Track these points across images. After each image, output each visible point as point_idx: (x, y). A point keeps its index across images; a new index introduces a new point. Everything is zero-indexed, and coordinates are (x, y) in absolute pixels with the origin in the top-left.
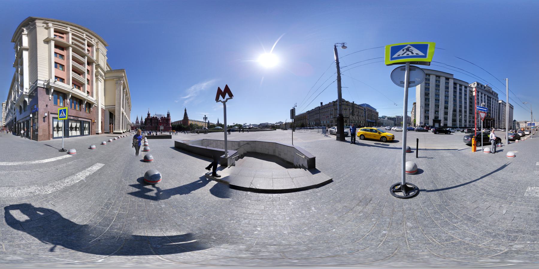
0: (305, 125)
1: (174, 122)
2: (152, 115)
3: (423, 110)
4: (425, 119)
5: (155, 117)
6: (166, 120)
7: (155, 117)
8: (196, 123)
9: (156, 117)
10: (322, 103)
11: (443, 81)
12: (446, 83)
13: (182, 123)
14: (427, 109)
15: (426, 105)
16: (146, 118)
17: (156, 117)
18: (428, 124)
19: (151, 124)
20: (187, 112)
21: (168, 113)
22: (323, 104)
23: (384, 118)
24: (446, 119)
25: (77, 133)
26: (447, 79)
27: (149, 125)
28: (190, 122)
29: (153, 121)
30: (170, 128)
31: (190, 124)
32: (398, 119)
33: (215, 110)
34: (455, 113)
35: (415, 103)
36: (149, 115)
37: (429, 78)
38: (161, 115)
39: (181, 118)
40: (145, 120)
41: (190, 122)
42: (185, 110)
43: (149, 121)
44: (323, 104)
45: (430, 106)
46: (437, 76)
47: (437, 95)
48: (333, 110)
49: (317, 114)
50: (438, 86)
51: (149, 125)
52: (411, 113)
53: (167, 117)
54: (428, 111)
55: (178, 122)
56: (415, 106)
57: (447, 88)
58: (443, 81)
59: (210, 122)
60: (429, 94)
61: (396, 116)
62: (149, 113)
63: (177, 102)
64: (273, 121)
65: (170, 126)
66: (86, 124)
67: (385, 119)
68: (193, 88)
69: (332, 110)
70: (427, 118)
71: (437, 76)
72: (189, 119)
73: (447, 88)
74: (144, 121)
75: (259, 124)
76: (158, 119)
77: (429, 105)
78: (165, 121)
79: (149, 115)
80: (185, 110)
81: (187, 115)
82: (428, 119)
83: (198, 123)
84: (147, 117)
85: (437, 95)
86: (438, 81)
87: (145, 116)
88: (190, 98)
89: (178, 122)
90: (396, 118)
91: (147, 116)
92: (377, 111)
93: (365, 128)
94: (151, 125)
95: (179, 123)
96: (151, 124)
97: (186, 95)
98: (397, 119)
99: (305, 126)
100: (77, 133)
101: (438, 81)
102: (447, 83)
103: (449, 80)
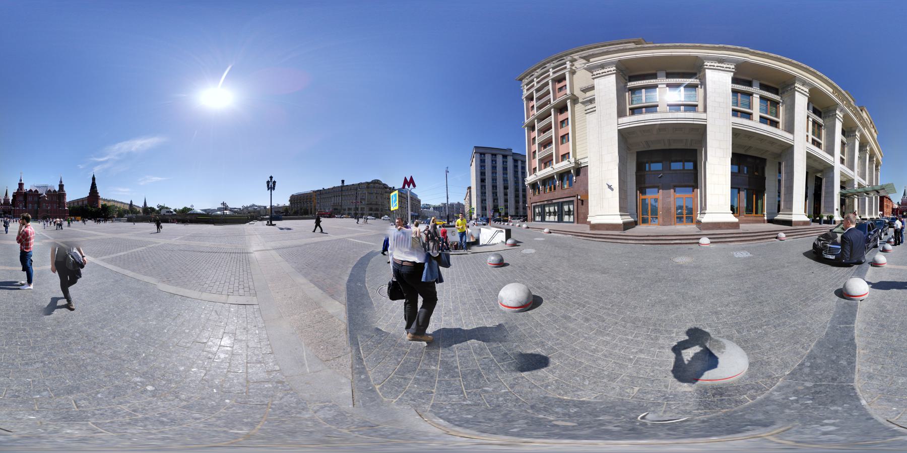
0: (309, 211)
1: (73, 202)
2: (27, 187)
3: (479, 200)
4: (482, 210)
5: (33, 190)
6: (58, 195)
7: (33, 190)
8: (113, 203)
9: (36, 191)
10: (343, 181)
11: (500, 159)
12: (503, 162)
13: (86, 202)
14: (484, 198)
15: (482, 193)
16: (14, 193)
17: (36, 191)
18: (486, 215)
19: (26, 204)
20: (97, 182)
21: (61, 182)
22: (345, 184)
23: (429, 209)
24: (506, 207)
25: (549, 209)
26: (505, 157)
27: (21, 206)
28: (101, 203)
29: (30, 199)
30: (65, 213)
31: (103, 206)
32: (445, 208)
33: (142, 184)
34: (517, 199)
35: (470, 188)
36: (21, 185)
37: (484, 158)
38: (46, 187)
39: (85, 193)
40: (13, 196)
41: (101, 203)
42: (94, 179)
43: (21, 198)
44: (345, 184)
45: (487, 195)
46: (492, 155)
47: (494, 180)
48: (366, 194)
49: (337, 196)
50: (494, 168)
51: (21, 206)
52: (465, 199)
53: (59, 191)
54: (485, 200)
55: (78, 201)
56: (470, 192)
57: (505, 169)
58: (500, 159)
59: (133, 204)
60: (485, 179)
61: (442, 204)
62: (22, 182)
63: (81, 167)
64: (237, 203)
65: (66, 208)
66: (550, 208)
67: (431, 210)
68: (117, 146)
69: (365, 193)
70: (484, 209)
71: (492, 155)
72: (99, 195)
73: (505, 169)
74: (11, 198)
75: (181, 208)
76: (42, 194)
77: (485, 193)
78: (55, 199)
79: (21, 185)
80: (94, 179)
81: (95, 184)
82: (486, 210)
83: (116, 204)
84: (18, 190)
85: (494, 180)
86: (494, 161)
87: (14, 188)
88: (106, 162)
89: (78, 202)
90: (442, 207)
91: (17, 187)
92: (419, 198)
93: (157, 245)
94: (26, 207)
95: (80, 203)
96: (26, 204)
97: (101, 156)
98: (443, 209)
99: (309, 213)
100: (549, 209)
101: (494, 161)
102: (505, 162)
103: (506, 158)
